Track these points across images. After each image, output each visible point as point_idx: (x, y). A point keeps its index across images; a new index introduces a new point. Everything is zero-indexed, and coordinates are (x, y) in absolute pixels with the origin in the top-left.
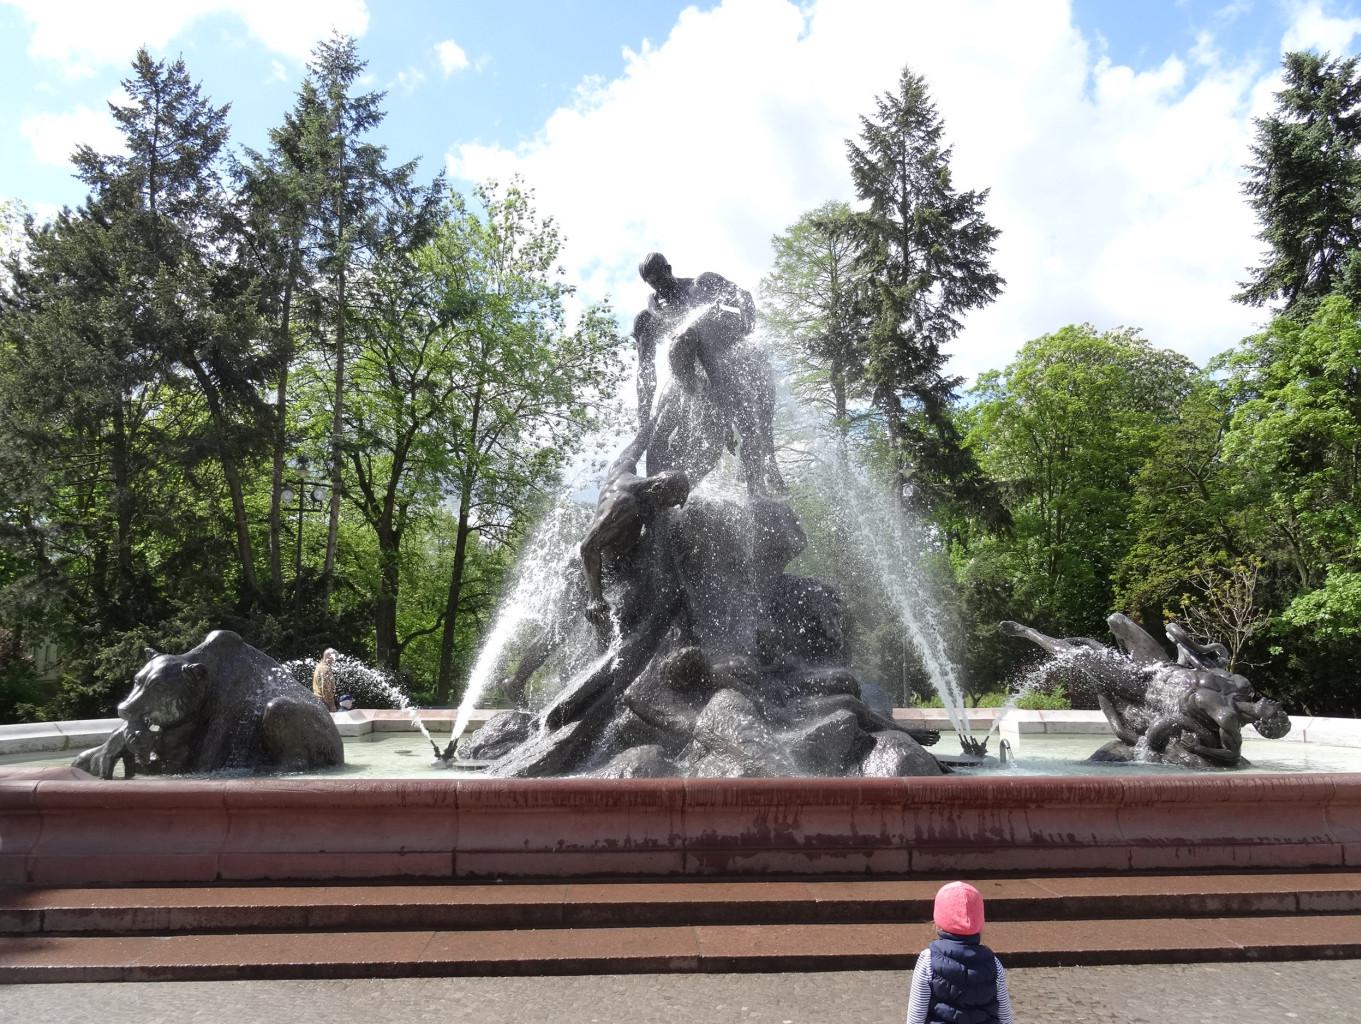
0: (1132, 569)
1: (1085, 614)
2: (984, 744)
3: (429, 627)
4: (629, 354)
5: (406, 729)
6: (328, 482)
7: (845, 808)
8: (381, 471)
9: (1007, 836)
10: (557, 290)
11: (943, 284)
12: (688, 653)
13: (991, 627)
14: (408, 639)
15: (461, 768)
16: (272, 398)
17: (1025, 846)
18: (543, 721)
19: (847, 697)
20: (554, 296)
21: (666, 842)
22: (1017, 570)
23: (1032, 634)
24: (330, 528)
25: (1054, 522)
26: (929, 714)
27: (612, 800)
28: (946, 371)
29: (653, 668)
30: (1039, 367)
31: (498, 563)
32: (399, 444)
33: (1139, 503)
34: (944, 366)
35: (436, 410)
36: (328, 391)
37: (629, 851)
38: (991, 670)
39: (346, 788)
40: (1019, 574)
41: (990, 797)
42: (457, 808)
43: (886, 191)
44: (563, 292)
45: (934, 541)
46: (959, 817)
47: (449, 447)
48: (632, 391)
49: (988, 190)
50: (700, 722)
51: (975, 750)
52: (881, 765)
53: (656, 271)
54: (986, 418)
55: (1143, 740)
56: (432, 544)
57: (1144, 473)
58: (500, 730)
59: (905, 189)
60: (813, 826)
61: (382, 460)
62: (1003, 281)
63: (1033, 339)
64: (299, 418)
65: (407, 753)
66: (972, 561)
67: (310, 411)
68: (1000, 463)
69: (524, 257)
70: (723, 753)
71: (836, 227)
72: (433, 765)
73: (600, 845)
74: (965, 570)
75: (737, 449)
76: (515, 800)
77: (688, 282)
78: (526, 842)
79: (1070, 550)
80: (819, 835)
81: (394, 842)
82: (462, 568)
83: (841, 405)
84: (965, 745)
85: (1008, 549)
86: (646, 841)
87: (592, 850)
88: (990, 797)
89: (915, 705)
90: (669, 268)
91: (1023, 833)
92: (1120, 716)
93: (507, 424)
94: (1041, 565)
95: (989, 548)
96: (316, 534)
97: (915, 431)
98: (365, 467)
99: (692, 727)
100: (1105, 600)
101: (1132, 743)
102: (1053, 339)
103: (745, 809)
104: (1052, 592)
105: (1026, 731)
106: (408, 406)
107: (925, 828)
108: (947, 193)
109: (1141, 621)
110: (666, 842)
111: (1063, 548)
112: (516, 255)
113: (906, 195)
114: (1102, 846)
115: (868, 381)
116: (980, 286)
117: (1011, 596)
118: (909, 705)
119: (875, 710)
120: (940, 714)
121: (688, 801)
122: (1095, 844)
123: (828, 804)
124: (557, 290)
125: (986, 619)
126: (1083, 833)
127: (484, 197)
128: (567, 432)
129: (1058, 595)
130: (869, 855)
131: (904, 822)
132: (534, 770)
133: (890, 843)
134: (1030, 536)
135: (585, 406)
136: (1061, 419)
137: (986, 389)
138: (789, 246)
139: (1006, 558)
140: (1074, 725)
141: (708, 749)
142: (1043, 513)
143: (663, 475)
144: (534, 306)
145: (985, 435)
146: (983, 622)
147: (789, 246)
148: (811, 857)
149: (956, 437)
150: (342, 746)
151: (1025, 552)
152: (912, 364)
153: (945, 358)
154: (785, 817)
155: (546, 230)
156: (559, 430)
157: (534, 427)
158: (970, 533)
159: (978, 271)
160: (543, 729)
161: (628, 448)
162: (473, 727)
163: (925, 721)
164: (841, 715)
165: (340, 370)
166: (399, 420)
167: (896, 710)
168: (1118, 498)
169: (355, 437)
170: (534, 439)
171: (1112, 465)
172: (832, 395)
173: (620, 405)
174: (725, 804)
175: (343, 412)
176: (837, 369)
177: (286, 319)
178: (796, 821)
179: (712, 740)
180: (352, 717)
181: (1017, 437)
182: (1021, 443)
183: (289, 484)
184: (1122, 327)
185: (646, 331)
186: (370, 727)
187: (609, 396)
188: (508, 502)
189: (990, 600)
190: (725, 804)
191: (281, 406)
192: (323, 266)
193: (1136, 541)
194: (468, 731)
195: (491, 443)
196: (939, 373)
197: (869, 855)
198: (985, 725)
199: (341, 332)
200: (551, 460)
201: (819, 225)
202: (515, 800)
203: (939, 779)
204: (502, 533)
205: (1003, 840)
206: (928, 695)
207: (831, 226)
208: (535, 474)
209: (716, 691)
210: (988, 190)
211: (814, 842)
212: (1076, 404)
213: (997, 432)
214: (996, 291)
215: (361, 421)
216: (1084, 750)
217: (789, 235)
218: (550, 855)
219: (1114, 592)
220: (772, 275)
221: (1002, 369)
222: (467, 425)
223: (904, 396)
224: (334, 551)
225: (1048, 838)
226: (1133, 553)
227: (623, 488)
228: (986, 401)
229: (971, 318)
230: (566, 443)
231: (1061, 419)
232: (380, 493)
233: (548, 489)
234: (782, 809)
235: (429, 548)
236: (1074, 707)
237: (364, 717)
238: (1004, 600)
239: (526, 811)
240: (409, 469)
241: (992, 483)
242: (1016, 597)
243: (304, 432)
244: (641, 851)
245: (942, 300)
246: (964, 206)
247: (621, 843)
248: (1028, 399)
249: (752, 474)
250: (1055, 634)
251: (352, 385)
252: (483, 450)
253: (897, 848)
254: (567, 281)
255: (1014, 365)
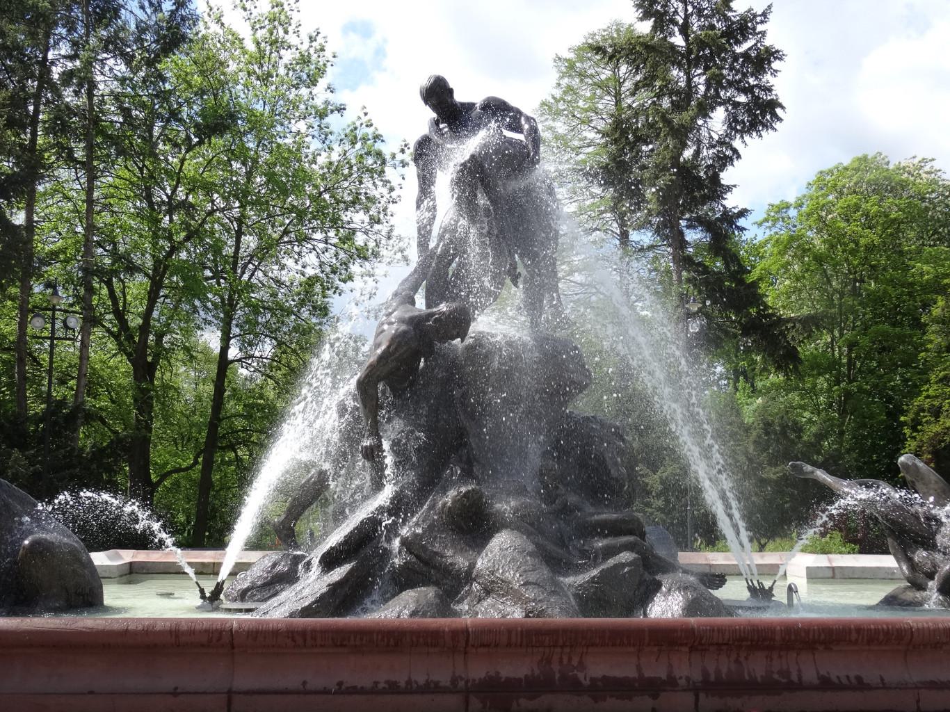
0: (923, 411)
1: (875, 457)
2: (771, 588)
3: (184, 465)
4: (406, 179)
5: (173, 571)
6: (77, 308)
7: (631, 649)
8: (135, 298)
9: (794, 677)
10: (326, 109)
11: (727, 110)
12: (468, 492)
13: (779, 468)
14: (163, 477)
15: (229, 610)
16: (19, 218)
17: (811, 687)
18: (316, 562)
19: (631, 538)
20: (322, 115)
21: (448, 684)
22: (805, 410)
23: (821, 475)
24: (81, 358)
25: (845, 361)
26: (716, 559)
27: (393, 640)
28: (732, 201)
29: (432, 507)
30: (831, 198)
31: (261, 397)
32: (155, 269)
33: (931, 342)
34: (728, 196)
35: (193, 234)
36: (78, 212)
37: (412, 693)
38: (781, 512)
39: (116, 627)
40: (807, 414)
41: (778, 638)
42: (233, 648)
43: (666, 13)
44: (332, 111)
45: (720, 379)
46: (746, 658)
47: (208, 273)
48: (413, 215)
49: (770, 7)
50: (481, 563)
51: (761, 594)
52: (666, 607)
53: (437, 94)
54: (776, 250)
55: (933, 585)
56: (187, 377)
57: (936, 312)
58: (270, 572)
59: (686, 10)
60: (599, 667)
61: (137, 286)
62: (783, 108)
63: (826, 168)
64: (48, 241)
65: (169, 595)
66: (760, 400)
67: (60, 234)
68: (789, 298)
69: (291, 73)
70: (503, 596)
71: (615, 51)
72: (198, 608)
73: (381, 686)
74: (752, 407)
75: (520, 280)
76: (294, 640)
77: (470, 106)
78: (304, 683)
79: (860, 390)
80: (604, 676)
81: (168, 682)
82: (222, 403)
83: (624, 236)
84: (751, 589)
85: (796, 388)
86: (428, 683)
87: (374, 691)
88: (778, 638)
89: (698, 550)
90: (451, 91)
91: (810, 675)
92: (910, 561)
93: (266, 250)
94: (830, 405)
95: (776, 387)
96: (65, 365)
97: (700, 264)
98: (118, 293)
99: (472, 566)
100: (898, 443)
101: (921, 587)
102: (846, 169)
103: (530, 650)
104: (842, 433)
105: (814, 575)
106: (165, 230)
107: (711, 669)
108: (730, 14)
109: (932, 465)
110: (448, 684)
111: (854, 387)
112: (282, 71)
113: (687, 17)
114: (890, 688)
115: (650, 214)
116: (761, 113)
117: (800, 437)
118: (693, 550)
119: (661, 552)
120: (726, 559)
121: (471, 641)
122: (884, 686)
123: (614, 645)
124: (326, 109)
125: (774, 461)
126: (871, 674)
127: (245, 9)
128: (334, 261)
129: (847, 436)
130: (655, 697)
131: (690, 663)
132: (306, 612)
133: (677, 685)
134: (820, 374)
135: (354, 231)
136: (853, 252)
137: (775, 221)
138: (571, 66)
139: (794, 397)
140: (864, 569)
141: (488, 592)
142: (833, 350)
143: (443, 307)
144: (302, 126)
145: (774, 268)
146: (770, 464)
147: (571, 66)
148: (596, 700)
149: (743, 270)
150: (101, 587)
151: (813, 391)
152: (695, 189)
153: (729, 188)
154: (570, 659)
155: (314, 44)
156: (328, 257)
157: (299, 254)
158: (757, 371)
159: (762, 95)
160: (316, 569)
161: (406, 280)
162: (240, 568)
163: (711, 566)
164: (626, 556)
165: (89, 191)
166: (154, 245)
167: (680, 554)
168: (911, 336)
169: (107, 261)
170: (299, 267)
171: (904, 302)
172: (615, 225)
173: (391, 231)
174: (509, 645)
175: (94, 235)
176: (617, 201)
177: (34, 134)
178: (581, 662)
179: (493, 582)
180: (110, 558)
181: (807, 270)
182: (812, 277)
183: (36, 310)
184: (914, 157)
185: (424, 151)
186: (128, 566)
187: (379, 222)
188: (272, 333)
189: (780, 437)
190: (509, 645)
191: (30, 225)
192: (68, 77)
193: (928, 381)
194: (233, 574)
195: (256, 269)
196: (724, 202)
197: (655, 697)
198: (772, 570)
199: (90, 149)
200: (318, 288)
201: (598, 49)
202: (294, 640)
203: (723, 620)
204: (264, 366)
205: (792, 682)
206: (710, 535)
207: (610, 50)
208: (302, 303)
209: (498, 530)
210: (770, 7)
211: (599, 683)
212: (870, 237)
213: (786, 266)
214: (774, 115)
215: (115, 244)
216: (872, 595)
217: (571, 56)
218: (330, 697)
219: (905, 434)
220: (554, 98)
221: (791, 199)
222: (228, 251)
223: (688, 227)
224: (84, 381)
225: (836, 681)
226: (925, 394)
227: (401, 321)
228: (776, 233)
229: (751, 148)
230: (334, 272)
231: (853, 252)
232: (135, 321)
233: (314, 320)
234: (567, 650)
235: (187, 383)
236: (862, 552)
237: (120, 557)
238: (793, 442)
239: (305, 651)
240: (166, 297)
241: (779, 318)
242: (805, 438)
243: (54, 255)
244: (423, 693)
245: (725, 128)
246: (744, 27)
247: (402, 684)
248: (819, 231)
249: (533, 305)
250: (844, 476)
251: (105, 206)
252: (246, 277)
253: (685, 690)
254: (336, 99)
255: (804, 196)
